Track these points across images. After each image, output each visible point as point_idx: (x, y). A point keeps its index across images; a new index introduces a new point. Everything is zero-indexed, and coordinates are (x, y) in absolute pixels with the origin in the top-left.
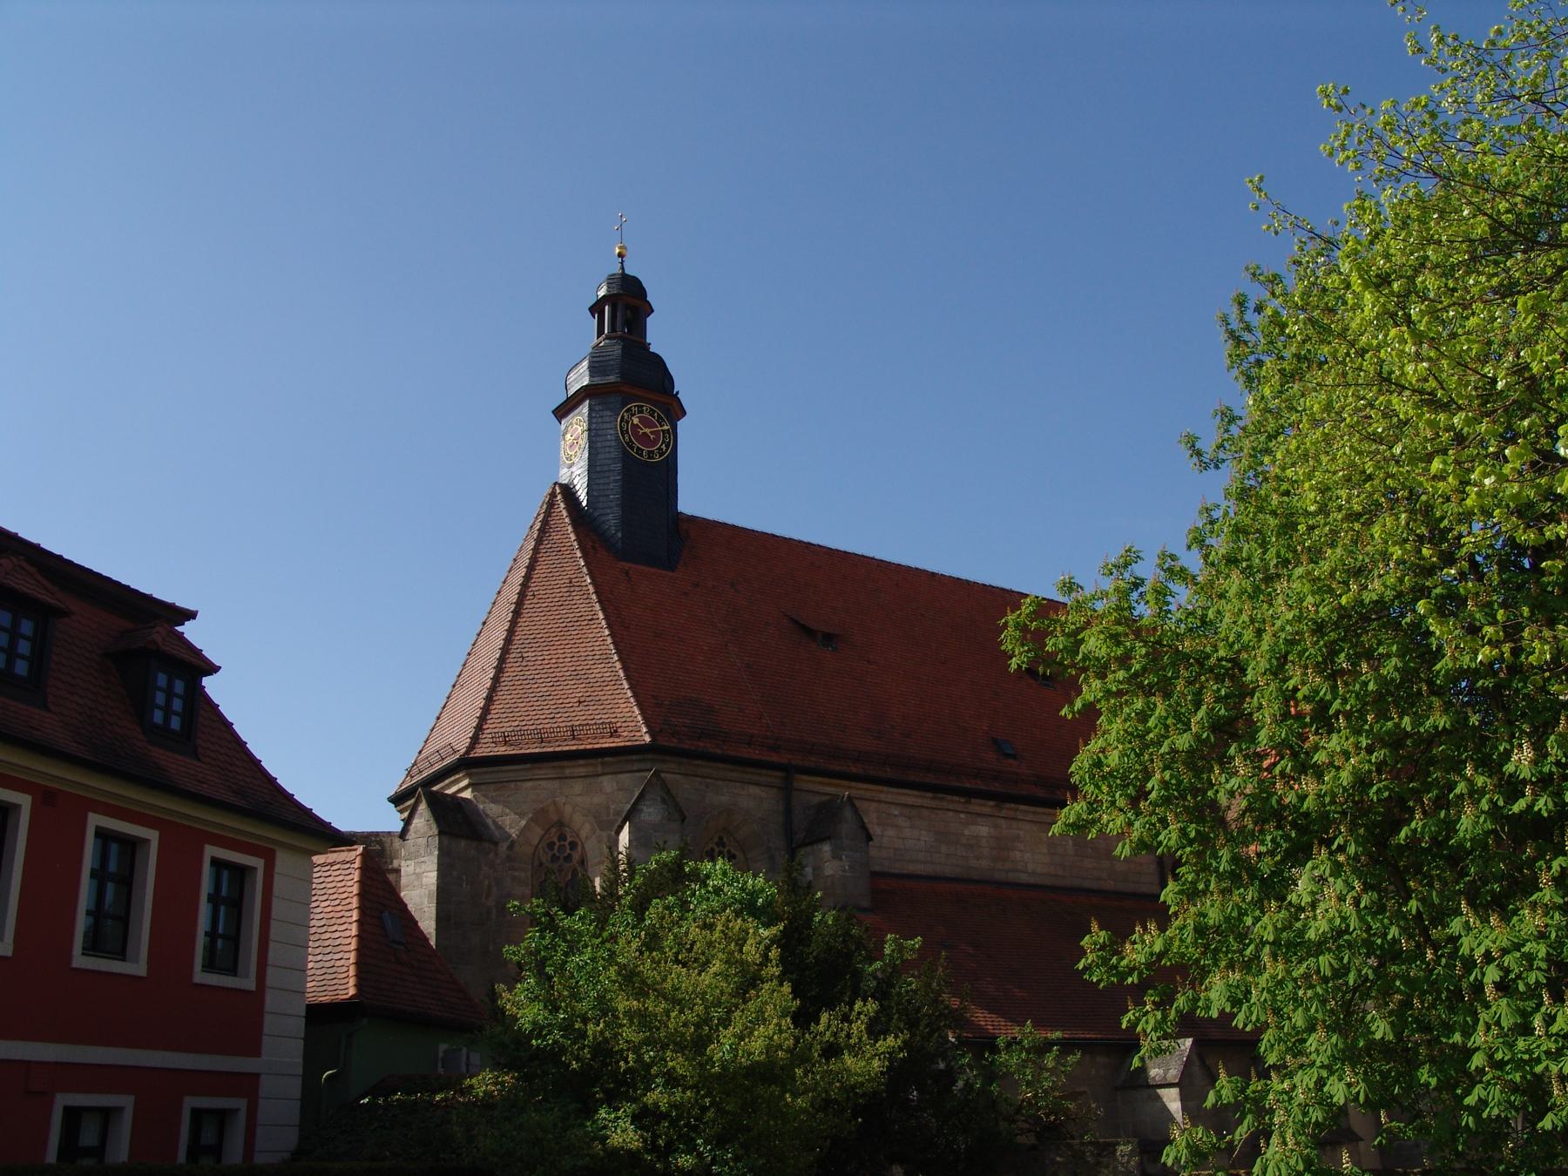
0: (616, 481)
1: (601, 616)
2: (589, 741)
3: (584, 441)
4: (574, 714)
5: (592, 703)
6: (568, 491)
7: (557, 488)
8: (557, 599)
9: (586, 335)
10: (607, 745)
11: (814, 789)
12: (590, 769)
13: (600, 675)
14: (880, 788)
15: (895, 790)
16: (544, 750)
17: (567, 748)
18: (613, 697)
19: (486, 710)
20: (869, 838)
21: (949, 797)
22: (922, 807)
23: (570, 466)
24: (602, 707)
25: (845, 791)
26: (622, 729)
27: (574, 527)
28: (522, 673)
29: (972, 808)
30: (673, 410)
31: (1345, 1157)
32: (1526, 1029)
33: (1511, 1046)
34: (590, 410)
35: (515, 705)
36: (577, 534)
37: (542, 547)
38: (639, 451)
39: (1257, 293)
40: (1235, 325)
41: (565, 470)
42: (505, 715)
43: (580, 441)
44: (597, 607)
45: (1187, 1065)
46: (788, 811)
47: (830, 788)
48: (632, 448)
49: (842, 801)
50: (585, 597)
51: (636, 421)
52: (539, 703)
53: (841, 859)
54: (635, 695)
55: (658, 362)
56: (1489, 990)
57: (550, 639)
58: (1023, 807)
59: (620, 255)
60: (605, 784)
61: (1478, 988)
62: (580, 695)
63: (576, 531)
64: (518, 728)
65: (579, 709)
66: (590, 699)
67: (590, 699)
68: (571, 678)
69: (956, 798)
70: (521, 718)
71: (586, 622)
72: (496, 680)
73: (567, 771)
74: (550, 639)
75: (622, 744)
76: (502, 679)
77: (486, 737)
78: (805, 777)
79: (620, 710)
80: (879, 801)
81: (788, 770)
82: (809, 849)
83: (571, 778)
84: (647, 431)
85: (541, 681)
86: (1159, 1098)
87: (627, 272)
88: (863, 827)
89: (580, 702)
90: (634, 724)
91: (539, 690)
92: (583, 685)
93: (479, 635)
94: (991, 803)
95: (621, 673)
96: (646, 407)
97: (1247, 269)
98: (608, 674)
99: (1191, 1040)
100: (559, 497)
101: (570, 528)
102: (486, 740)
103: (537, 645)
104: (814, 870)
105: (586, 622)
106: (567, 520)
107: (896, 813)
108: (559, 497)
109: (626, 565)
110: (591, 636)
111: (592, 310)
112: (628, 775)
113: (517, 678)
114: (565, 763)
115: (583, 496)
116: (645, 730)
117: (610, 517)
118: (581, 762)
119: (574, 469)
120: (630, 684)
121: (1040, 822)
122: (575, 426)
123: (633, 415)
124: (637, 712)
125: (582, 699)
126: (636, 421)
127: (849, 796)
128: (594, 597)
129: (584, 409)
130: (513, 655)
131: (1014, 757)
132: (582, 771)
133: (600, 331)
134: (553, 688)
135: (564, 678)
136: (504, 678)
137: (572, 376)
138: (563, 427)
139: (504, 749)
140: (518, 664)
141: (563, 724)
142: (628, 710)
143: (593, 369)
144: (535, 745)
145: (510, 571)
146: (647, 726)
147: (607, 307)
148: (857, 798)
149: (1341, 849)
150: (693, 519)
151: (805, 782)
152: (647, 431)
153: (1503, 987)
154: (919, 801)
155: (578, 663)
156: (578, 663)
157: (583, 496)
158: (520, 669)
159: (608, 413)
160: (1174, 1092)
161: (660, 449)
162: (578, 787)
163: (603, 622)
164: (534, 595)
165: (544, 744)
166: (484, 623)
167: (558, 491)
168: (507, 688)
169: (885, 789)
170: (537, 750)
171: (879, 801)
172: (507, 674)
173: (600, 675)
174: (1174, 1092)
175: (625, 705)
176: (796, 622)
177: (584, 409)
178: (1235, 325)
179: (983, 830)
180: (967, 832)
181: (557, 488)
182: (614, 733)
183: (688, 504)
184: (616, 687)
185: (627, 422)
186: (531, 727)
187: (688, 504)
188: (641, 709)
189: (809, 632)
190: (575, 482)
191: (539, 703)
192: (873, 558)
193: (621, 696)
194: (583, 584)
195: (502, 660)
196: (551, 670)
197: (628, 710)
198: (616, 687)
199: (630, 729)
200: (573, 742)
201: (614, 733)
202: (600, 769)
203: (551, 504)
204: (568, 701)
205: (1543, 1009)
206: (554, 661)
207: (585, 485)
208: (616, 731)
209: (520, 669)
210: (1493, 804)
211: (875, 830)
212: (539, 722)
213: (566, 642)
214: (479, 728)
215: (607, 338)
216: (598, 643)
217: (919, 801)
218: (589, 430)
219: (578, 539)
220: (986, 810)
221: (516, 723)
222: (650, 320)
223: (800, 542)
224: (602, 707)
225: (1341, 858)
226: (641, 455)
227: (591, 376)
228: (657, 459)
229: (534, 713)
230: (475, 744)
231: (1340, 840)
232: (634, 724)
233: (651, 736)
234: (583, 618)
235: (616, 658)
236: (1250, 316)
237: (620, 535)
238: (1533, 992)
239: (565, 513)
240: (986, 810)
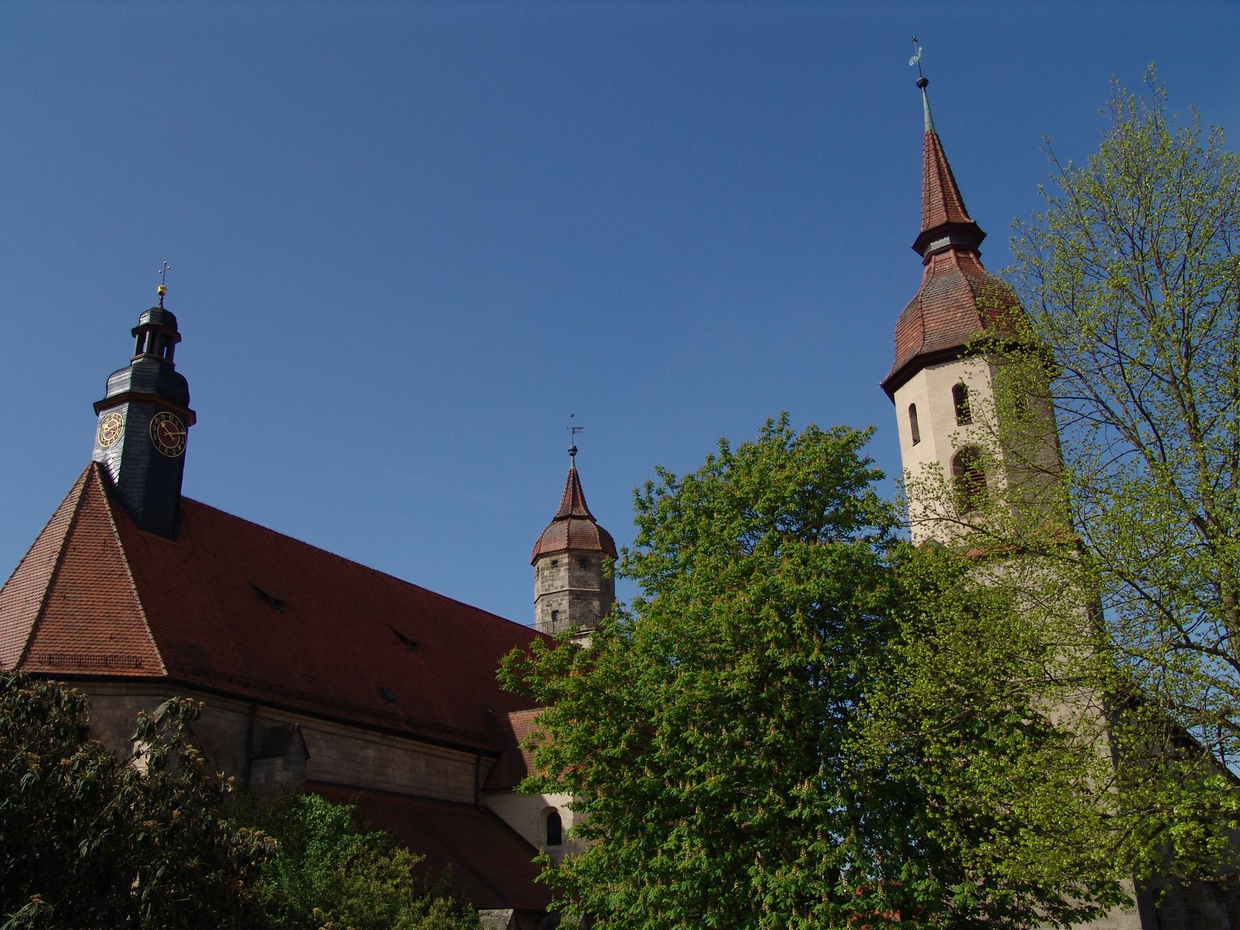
1: (129, 573)
2: (119, 669)
3: (121, 433)
4: (106, 647)
5: (121, 640)
6: (103, 469)
7: (95, 465)
8: (93, 555)
11: (271, 718)
13: (127, 619)
14: (310, 719)
16: (82, 672)
17: (100, 673)
18: (137, 637)
20: (308, 757)
21: (353, 728)
22: (335, 734)
23: (105, 449)
24: (129, 644)
25: (296, 721)
26: (145, 663)
28: (64, 609)
30: (189, 418)
34: (129, 411)
35: (58, 634)
36: (110, 505)
37: (81, 511)
39: (660, 483)
40: (643, 496)
41: (99, 451)
42: (49, 641)
43: (117, 433)
47: (281, 718)
48: (158, 445)
50: (116, 556)
51: (163, 425)
52: (77, 635)
53: (288, 771)
54: (155, 638)
55: (182, 382)
56: (765, 907)
57: (88, 585)
59: (161, 293)
61: (759, 904)
62: (111, 632)
63: (110, 503)
64: (61, 653)
65: (111, 643)
66: (119, 636)
67: (119, 636)
68: (104, 618)
69: (358, 729)
70: (63, 645)
71: (116, 576)
72: (42, 613)
74: (88, 585)
75: (145, 675)
76: (48, 612)
77: (34, 656)
78: (264, 708)
79: (143, 648)
83: (100, 695)
84: (170, 434)
85: (80, 617)
87: (165, 307)
89: (111, 638)
90: (154, 660)
91: (77, 624)
92: (114, 625)
95: (144, 620)
96: (171, 415)
97: (656, 468)
98: (134, 619)
99: (512, 910)
101: (105, 501)
102: (33, 660)
103: (77, 588)
104: (266, 776)
105: (116, 576)
106: (103, 493)
107: (319, 737)
108: (97, 473)
110: (120, 587)
113: (60, 613)
115: (115, 474)
116: (163, 666)
119: (109, 452)
120: (151, 628)
121: (407, 750)
122: (113, 420)
123: (161, 420)
125: (113, 636)
126: (163, 425)
127: (299, 726)
128: (124, 557)
129: (125, 408)
130: (57, 594)
131: (392, 701)
133: (139, 350)
134: (90, 625)
135: (98, 618)
136: (49, 611)
137: (114, 380)
138: (101, 417)
139: (48, 668)
140: (60, 602)
142: (149, 648)
143: (134, 380)
144: (75, 668)
145: (49, 524)
146: (165, 663)
147: (148, 333)
150: (187, 500)
152: (170, 434)
153: (774, 907)
155: (110, 607)
156: (110, 607)
157: (115, 474)
158: (62, 606)
161: (177, 448)
163: (131, 579)
164: (75, 549)
165: (81, 668)
167: (96, 468)
168: (51, 620)
170: (76, 672)
172: (51, 609)
173: (127, 619)
175: (147, 645)
177: (125, 408)
178: (643, 496)
179: (371, 753)
181: (95, 465)
183: (187, 491)
184: (140, 630)
185: (157, 426)
186: (70, 653)
187: (187, 491)
188: (159, 649)
189: (264, 596)
190: (110, 462)
191: (77, 635)
192: (304, 543)
193: (143, 637)
194: (115, 546)
196: (88, 610)
197: (149, 648)
198: (140, 630)
199: (151, 663)
200: (106, 669)
201: (138, 666)
202: (124, 690)
203: (90, 478)
205: (792, 918)
206: (90, 603)
207: (119, 467)
208: (140, 664)
209: (62, 606)
211: (312, 751)
212: (77, 649)
213: (101, 589)
214: (27, 650)
215: (145, 357)
216: (126, 594)
219: (112, 511)
220: (375, 739)
221: (59, 649)
222: (177, 345)
223: (258, 526)
224: (129, 644)
226: (164, 452)
227: (133, 384)
228: (175, 456)
229: (74, 642)
230: (24, 661)
232: (154, 660)
233: (168, 671)
234: (114, 573)
235: (140, 607)
236: (653, 495)
237: (141, 509)
238: (788, 910)
239: (101, 487)
240: (375, 739)
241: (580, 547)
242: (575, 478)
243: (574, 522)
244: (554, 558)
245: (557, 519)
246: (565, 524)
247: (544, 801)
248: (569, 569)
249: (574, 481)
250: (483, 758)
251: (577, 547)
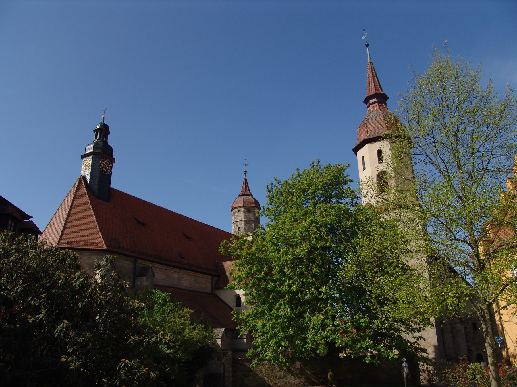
0: (98, 178)
1: (93, 214)
3: (90, 166)
6: (84, 178)
7: (82, 177)
9: (92, 137)
11: (142, 263)
12: (90, 253)
15: (158, 264)
16: (78, 247)
17: (84, 248)
20: (154, 277)
23: (85, 171)
25: (150, 265)
29: (174, 270)
30: (113, 161)
31: (281, 355)
33: (314, 338)
38: (104, 171)
39: (275, 183)
40: (270, 188)
41: (83, 172)
44: (92, 211)
46: (135, 268)
49: (149, 267)
51: (104, 163)
55: (110, 148)
56: (310, 328)
58: (185, 271)
59: (103, 118)
63: (87, 190)
72: (65, 227)
75: (99, 248)
77: (62, 242)
78: (139, 260)
81: (136, 258)
82: (140, 278)
84: (107, 166)
88: (153, 274)
93: (56, 212)
101: (85, 189)
106: (84, 186)
108: (82, 180)
109: (99, 200)
112: (99, 256)
114: (83, 251)
115: (88, 180)
116: (105, 245)
118: (88, 251)
119: (86, 172)
126: (104, 163)
129: (91, 157)
132: (87, 254)
133: (96, 137)
137: (87, 147)
138: (83, 160)
143: (94, 148)
145: (66, 197)
146: (106, 244)
148: (153, 267)
150: (113, 189)
151: (139, 261)
152: (107, 166)
157: (88, 180)
160: (220, 340)
161: (109, 171)
162: (86, 257)
163: (94, 216)
170: (76, 247)
174: (220, 340)
176: (136, 219)
177: (91, 157)
178: (270, 188)
179: (176, 275)
180: (172, 276)
182: (97, 245)
183: (113, 185)
187: (113, 185)
189: (139, 222)
190: (86, 176)
195: (66, 222)
201: (97, 245)
202: (92, 254)
203: (80, 181)
214: (60, 239)
220: (177, 271)
233: (107, 247)
235: (97, 225)
236: (273, 187)
237: (97, 192)
239: (84, 184)
240: (177, 271)
242: (246, 182)
243: (245, 196)
244: (238, 209)
245: (240, 196)
246: (243, 197)
247: (235, 292)
248: (244, 213)
249: (245, 182)
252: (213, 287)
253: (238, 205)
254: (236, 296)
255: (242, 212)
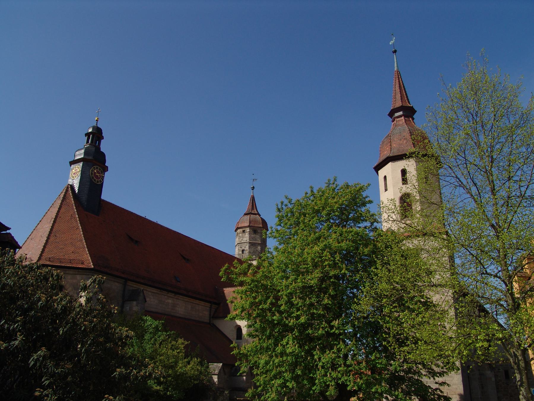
1: (80, 228)
3: (79, 174)
6: (72, 187)
7: (69, 186)
10: (80, 266)
11: (133, 286)
14: (148, 287)
15: (151, 288)
16: (61, 265)
19: (43, 250)
20: (146, 301)
21: (164, 291)
25: (142, 287)
27: (73, 199)
30: (105, 169)
32: (326, 375)
36: (74, 201)
41: (71, 180)
44: (79, 225)
45: (220, 370)
48: (93, 179)
51: (95, 171)
54: (89, 253)
55: (103, 155)
58: (181, 296)
59: (97, 120)
60: (78, 277)
63: (74, 200)
69: (165, 292)
73: (67, 272)
75: (85, 267)
77: (43, 258)
78: (130, 282)
80: (147, 291)
84: (98, 175)
86: (212, 377)
87: (98, 126)
89: (73, 252)
94: (173, 294)
95: (86, 246)
100: (69, 189)
102: (43, 259)
104: (130, 308)
108: (69, 189)
111: (86, 135)
114: (67, 270)
117: (84, 198)
118: (72, 270)
119: (74, 181)
123: (95, 169)
124: (90, 258)
126: (95, 171)
127: (143, 290)
131: (179, 282)
132: (71, 272)
133: (88, 142)
136: (50, 241)
137: (77, 153)
139: (49, 262)
141: (67, 258)
143: (85, 153)
149: (294, 334)
151: (130, 283)
152: (98, 175)
154: (156, 292)
159: (88, 167)
160: (216, 376)
161: (100, 180)
162: (69, 277)
166: (40, 221)
167: (69, 187)
169: (149, 287)
170: (59, 265)
171: (147, 291)
174: (216, 376)
177: (81, 164)
179: (170, 301)
180: (166, 301)
181: (69, 186)
183: (103, 197)
187: (103, 197)
189: (131, 238)
190: (75, 185)
201: (83, 263)
202: (77, 273)
203: (67, 191)
204: (69, 251)
210: (328, 330)
211: (147, 299)
214: (41, 255)
217: (156, 292)
218: (82, 171)
219: (75, 203)
225: (294, 336)
227: (84, 155)
228: (99, 183)
231: (294, 332)
233: (94, 266)
237: (86, 203)
238: (328, 368)
241: (254, 225)
243: (252, 215)
245: (245, 214)
246: (249, 216)
247: (236, 323)
248: (249, 234)
250: (213, 305)
251: (253, 225)
252: (211, 316)
253: (243, 225)
254: (237, 327)
255: (247, 232)
